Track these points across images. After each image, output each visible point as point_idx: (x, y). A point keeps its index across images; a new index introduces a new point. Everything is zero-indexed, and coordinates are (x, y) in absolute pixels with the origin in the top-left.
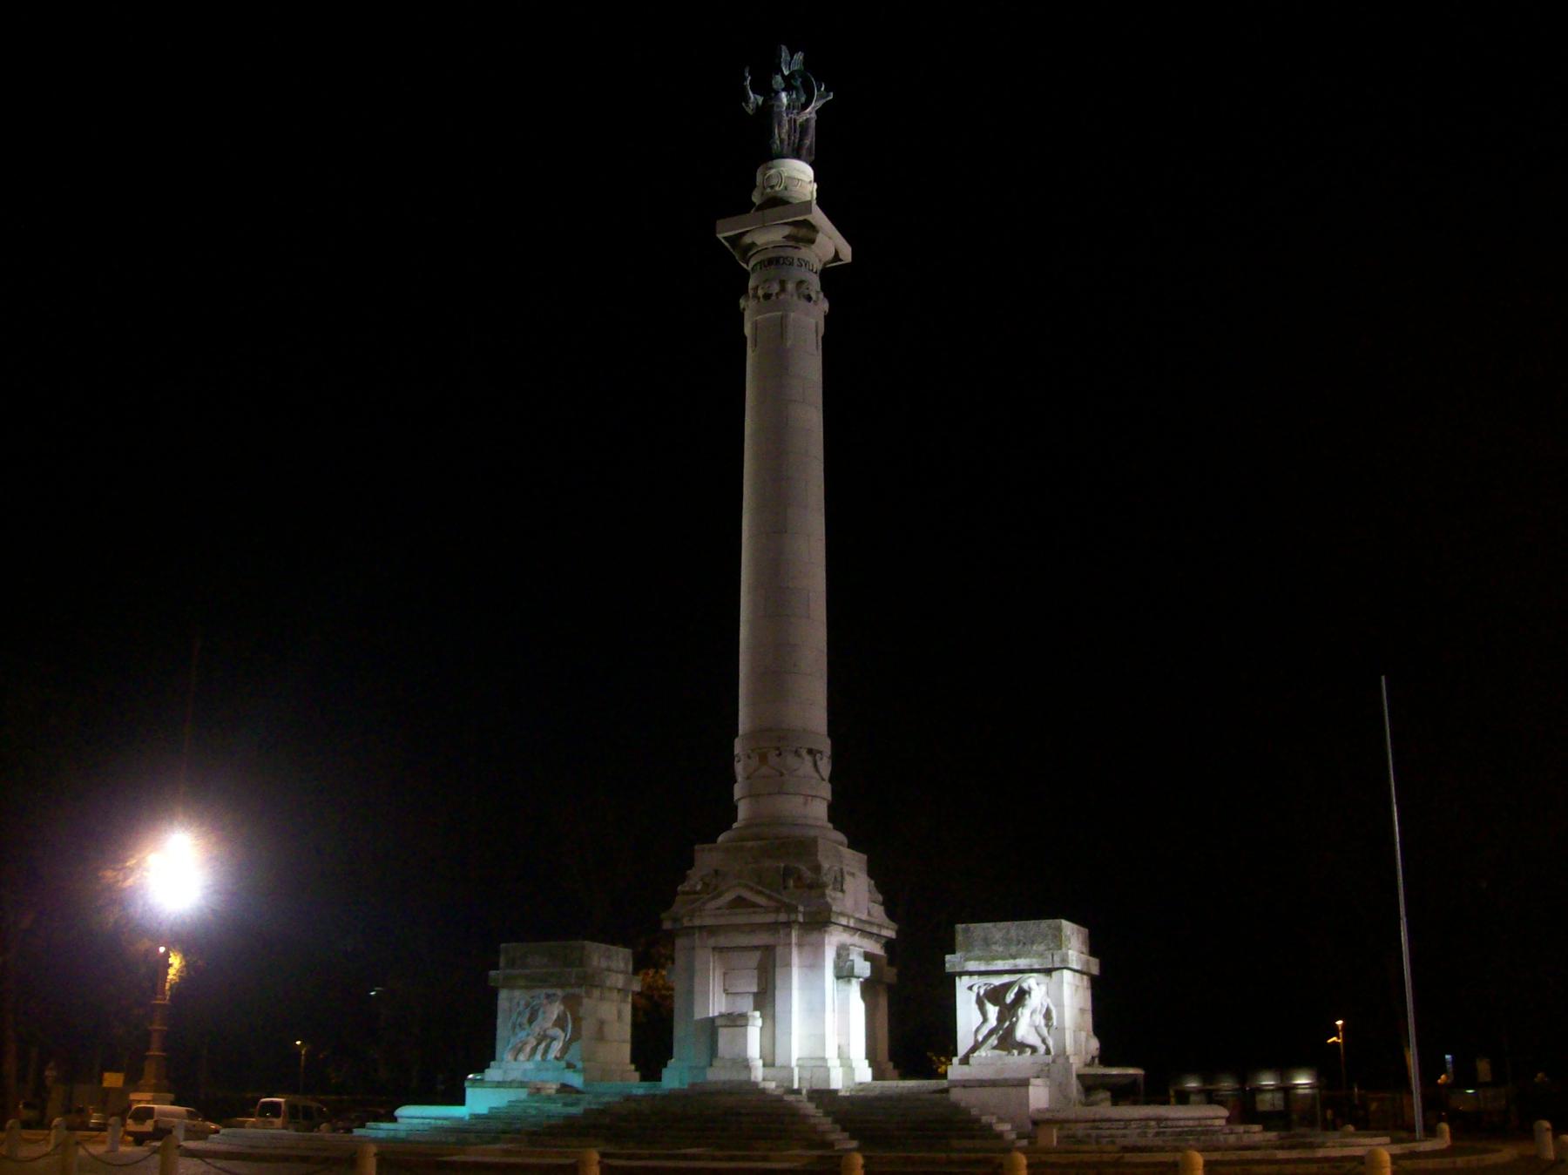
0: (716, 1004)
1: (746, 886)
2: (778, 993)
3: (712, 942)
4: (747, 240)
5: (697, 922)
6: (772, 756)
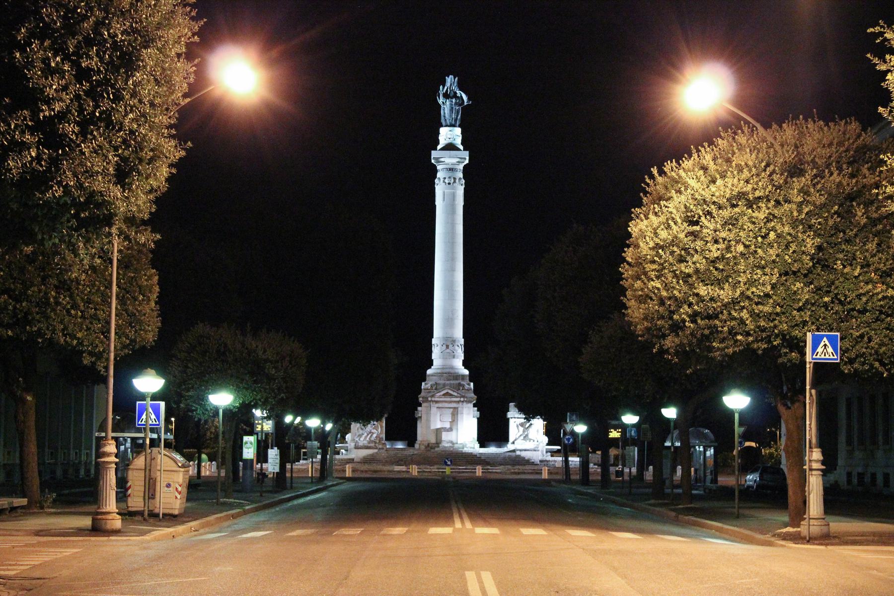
0: (437, 424)
1: (449, 389)
2: (459, 423)
3: (437, 405)
4: (442, 160)
5: (433, 399)
6: (451, 346)
